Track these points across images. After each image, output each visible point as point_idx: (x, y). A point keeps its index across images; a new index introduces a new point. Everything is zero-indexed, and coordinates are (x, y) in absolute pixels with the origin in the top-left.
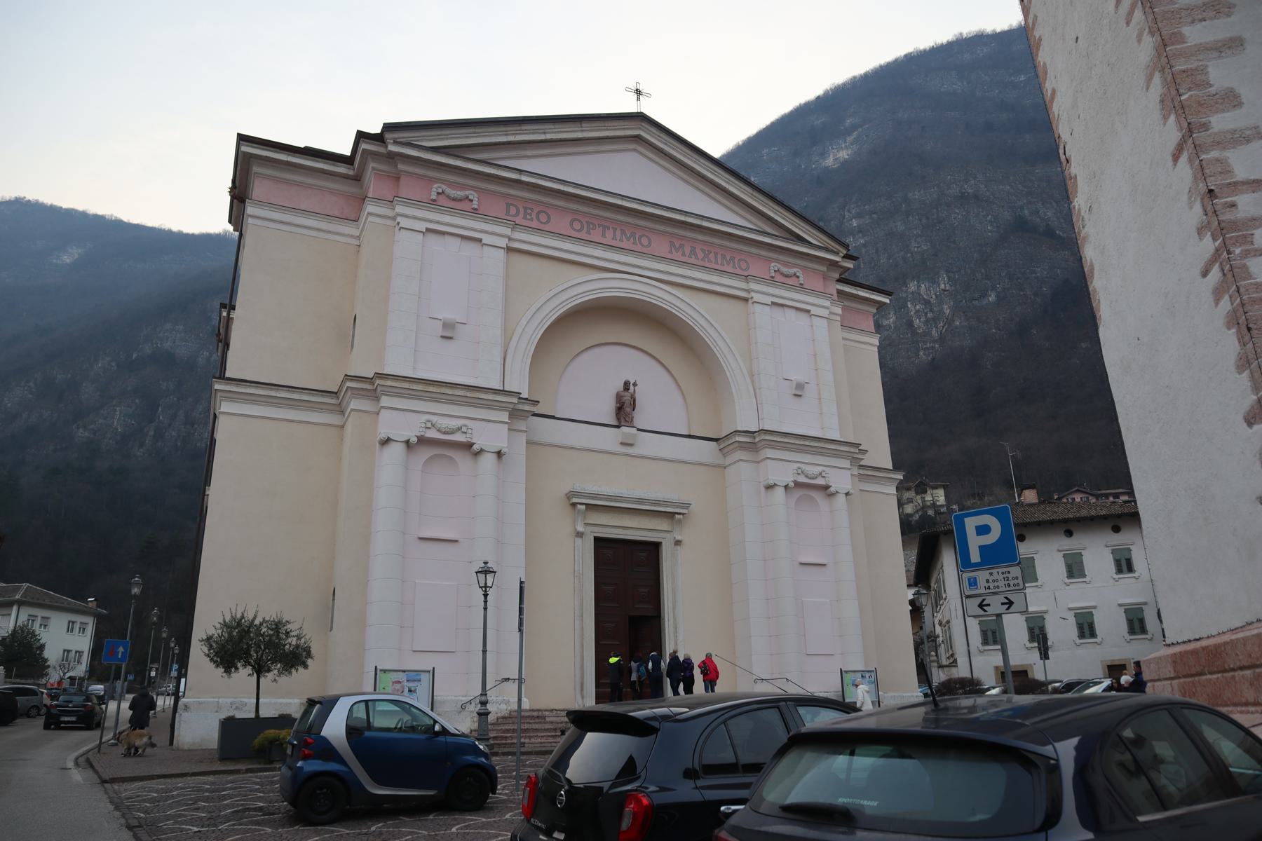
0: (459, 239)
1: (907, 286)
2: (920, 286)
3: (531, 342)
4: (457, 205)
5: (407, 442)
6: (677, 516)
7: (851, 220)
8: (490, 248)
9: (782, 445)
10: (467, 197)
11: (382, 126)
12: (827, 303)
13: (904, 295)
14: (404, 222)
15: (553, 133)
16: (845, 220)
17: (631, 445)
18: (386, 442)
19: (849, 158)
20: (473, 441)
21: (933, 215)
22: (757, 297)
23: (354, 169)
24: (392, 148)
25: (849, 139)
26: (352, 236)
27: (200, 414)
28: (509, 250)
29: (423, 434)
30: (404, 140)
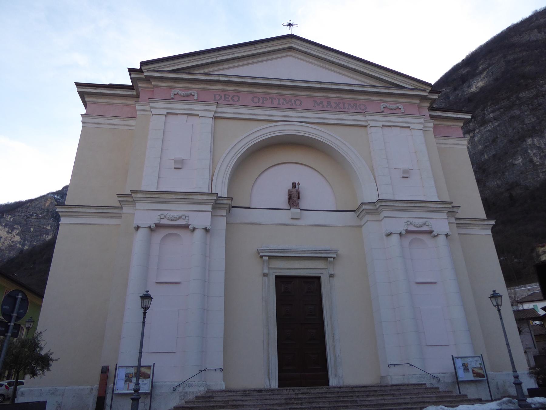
0: (399, 128)
1: (526, 142)
2: (534, 140)
3: (229, 165)
4: (187, 98)
5: (150, 227)
6: (329, 259)
7: (489, 114)
9: (394, 208)
10: (191, 94)
12: (422, 121)
13: (525, 147)
14: (154, 111)
15: (238, 53)
16: (486, 115)
18: (138, 228)
19: (484, 86)
20: (433, 230)
21: (535, 103)
22: (372, 124)
24: (147, 74)
25: (482, 76)
29: (406, 228)
30: (153, 69)
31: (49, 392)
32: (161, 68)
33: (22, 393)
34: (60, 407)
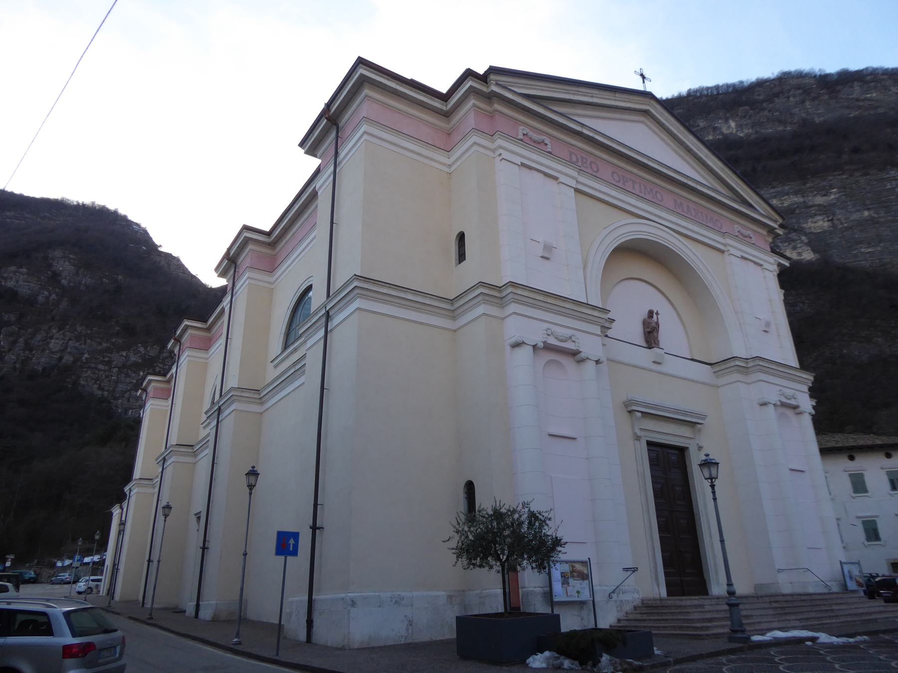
8: (566, 187)
11: (488, 67)
17: (659, 363)
20: (580, 350)
23: (446, 106)
24: (494, 88)
26: (444, 164)
27: (38, 342)
28: (577, 191)
29: (545, 340)
31: (392, 601)
32: (511, 86)
33: (353, 601)
34: (411, 625)
